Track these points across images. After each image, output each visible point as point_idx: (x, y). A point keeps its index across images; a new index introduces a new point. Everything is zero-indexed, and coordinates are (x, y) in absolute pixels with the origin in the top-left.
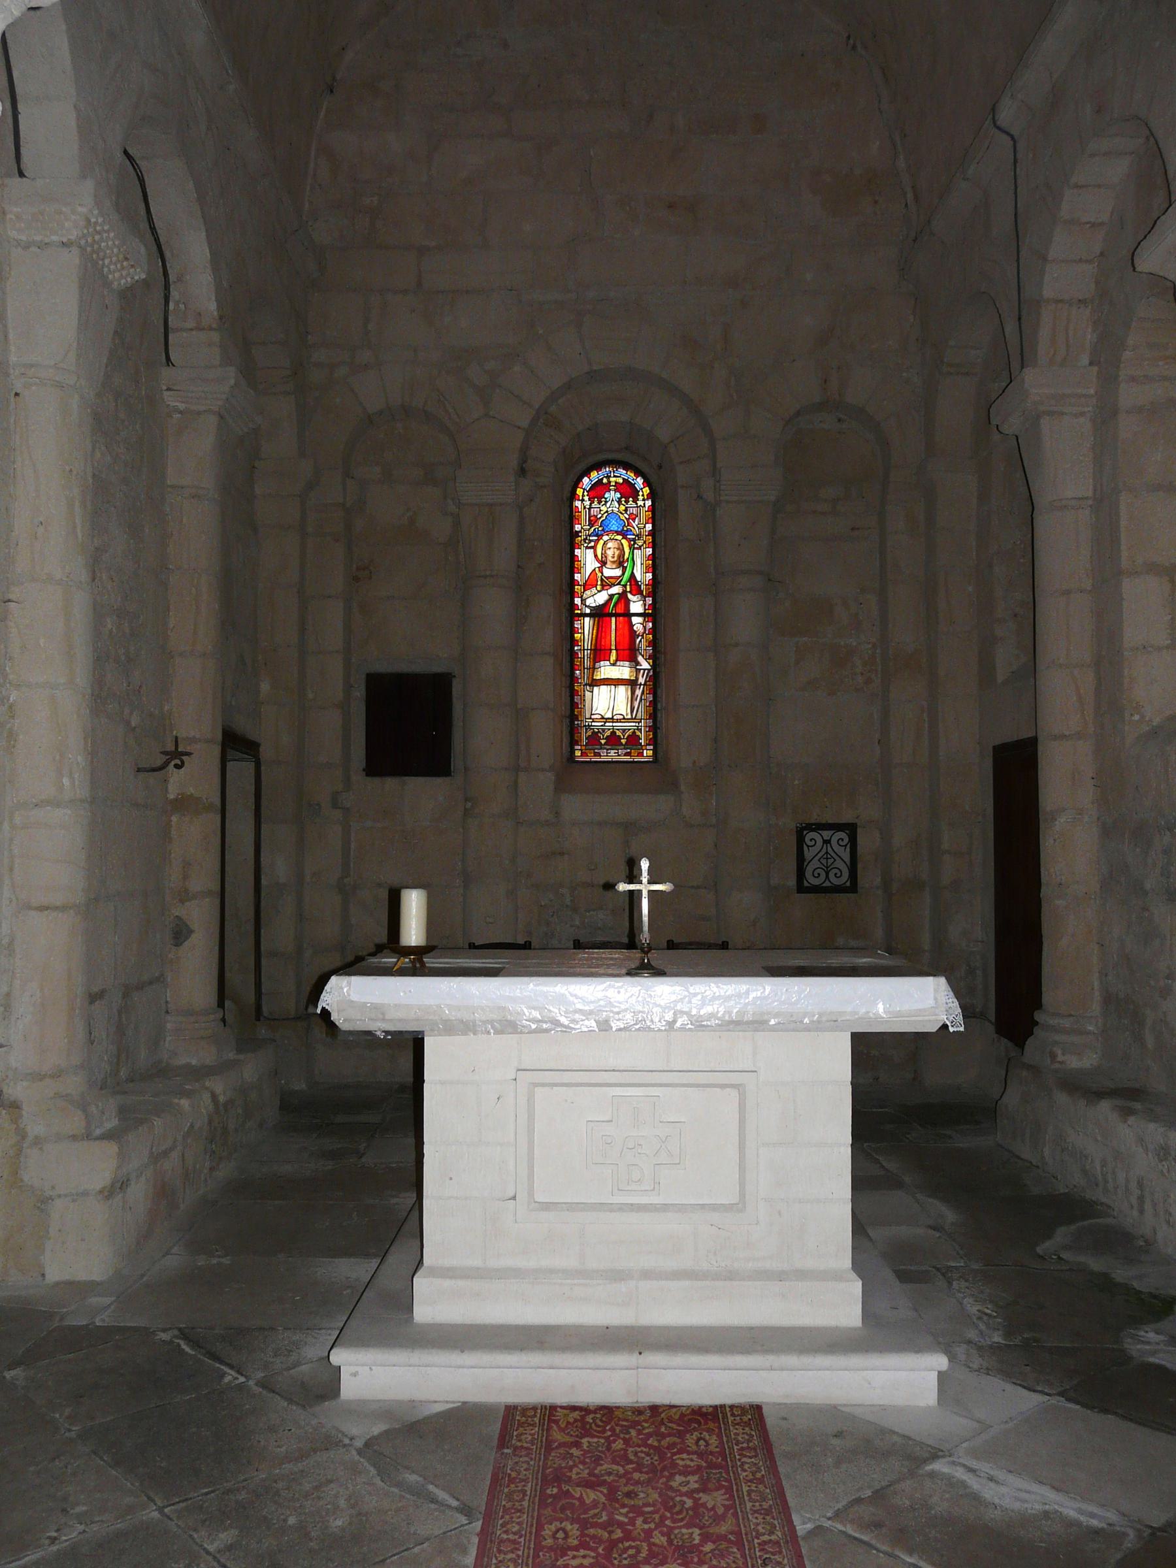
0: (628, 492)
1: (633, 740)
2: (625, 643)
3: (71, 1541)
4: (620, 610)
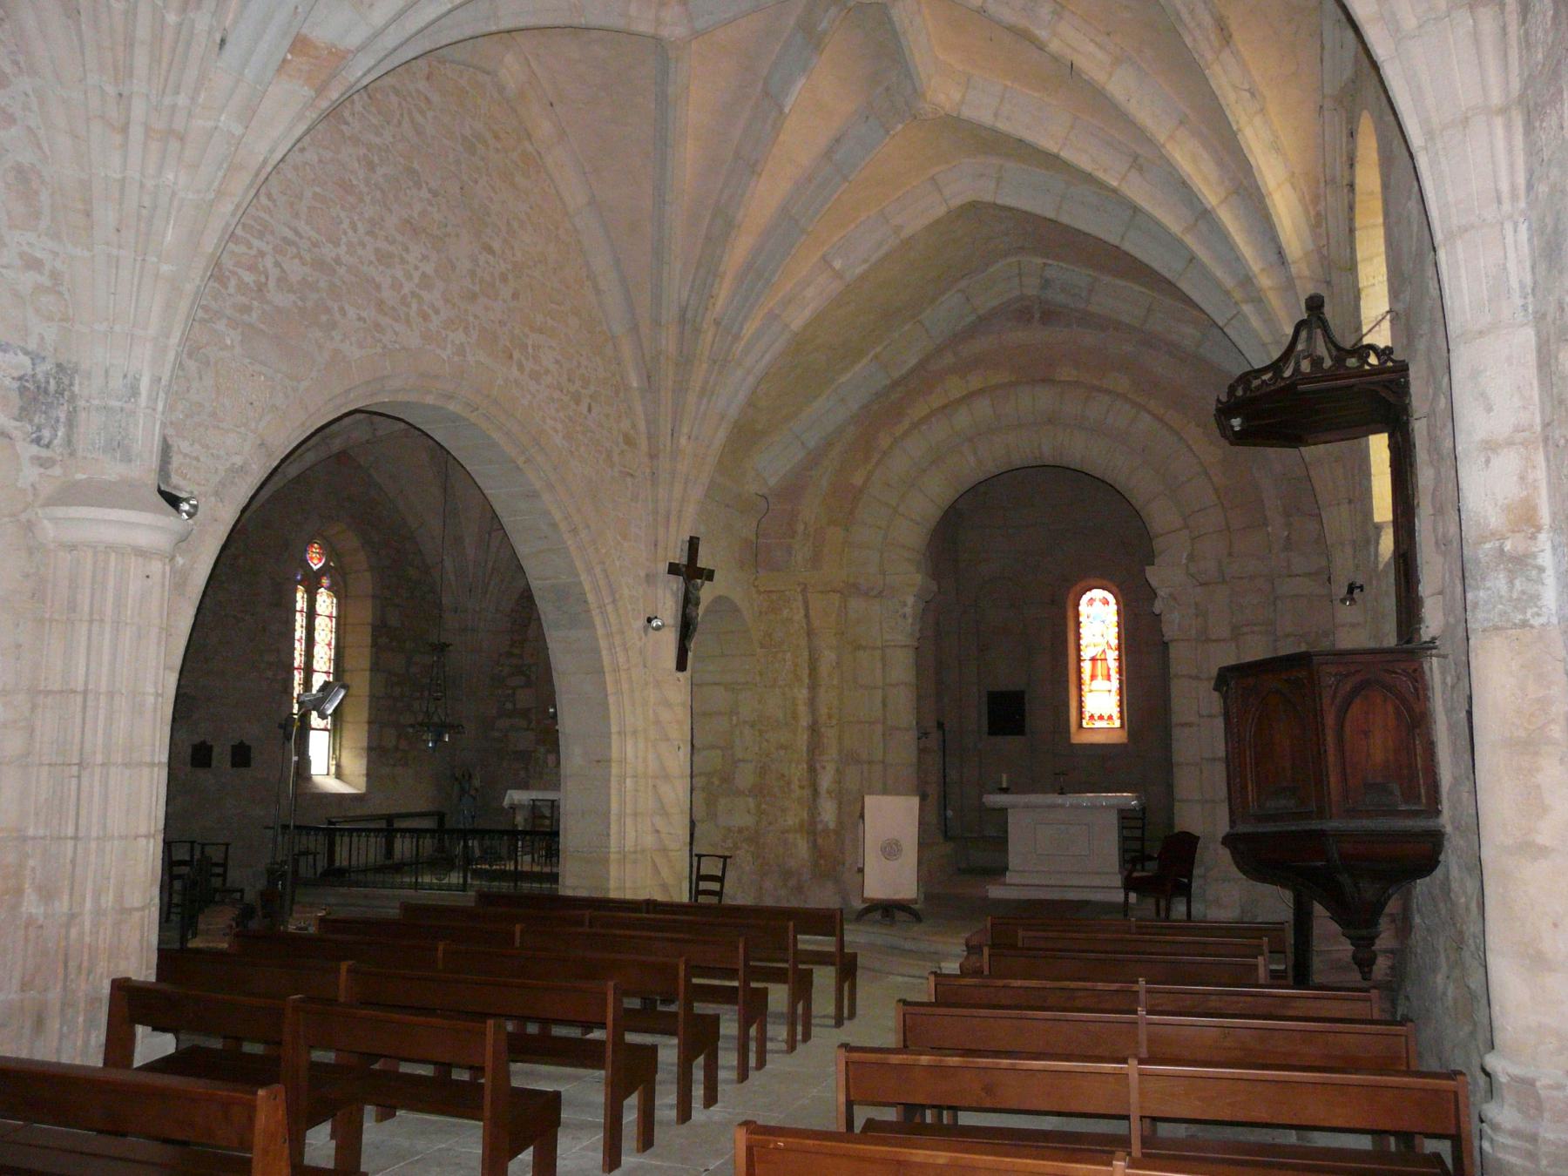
0: (1106, 602)
1: (1110, 718)
2: (1105, 672)
3: (906, 424)
4: (1103, 657)
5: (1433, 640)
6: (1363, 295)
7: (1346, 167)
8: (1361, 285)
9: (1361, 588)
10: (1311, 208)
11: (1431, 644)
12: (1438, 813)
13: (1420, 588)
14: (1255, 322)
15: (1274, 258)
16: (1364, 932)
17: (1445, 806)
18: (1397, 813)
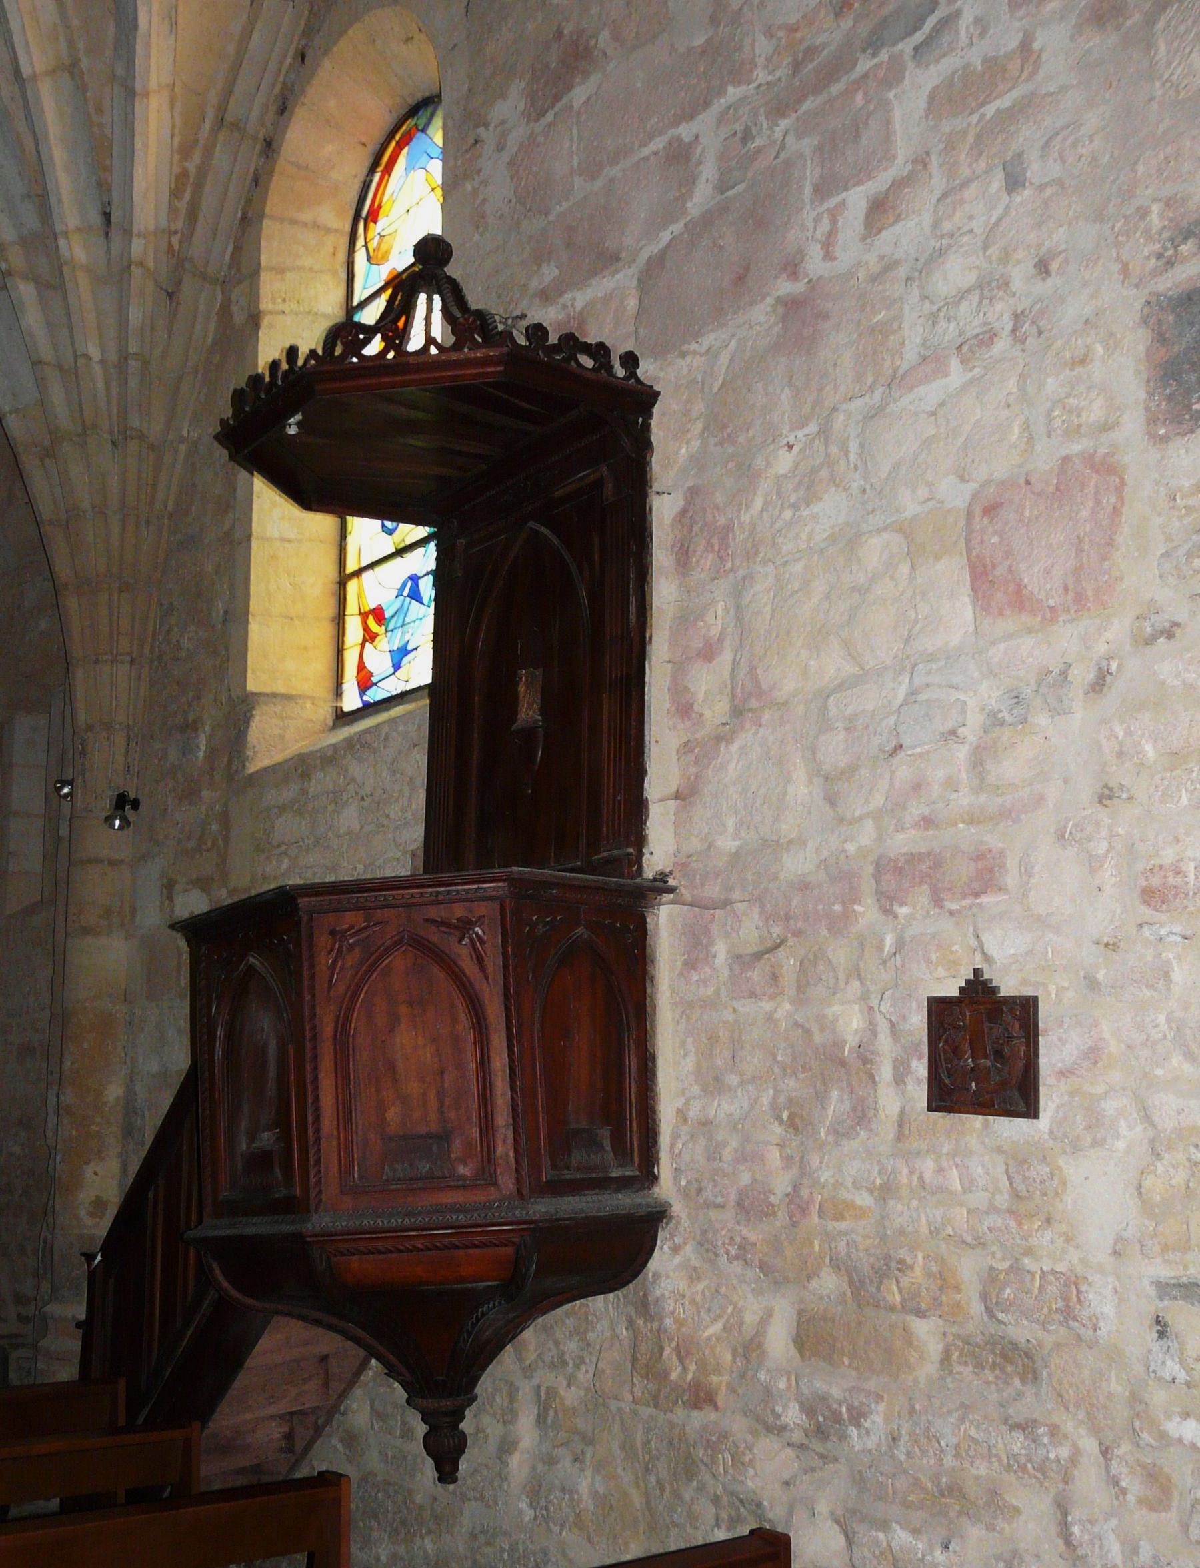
5: (662, 877)
6: (265, 322)
7: (273, 109)
8: (262, 307)
9: (135, 804)
10: (177, 157)
11: (661, 885)
12: (654, 1179)
13: (646, 784)
14: (33, 318)
15: (96, 218)
16: (447, 1404)
17: (665, 1169)
18: (603, 1184)
